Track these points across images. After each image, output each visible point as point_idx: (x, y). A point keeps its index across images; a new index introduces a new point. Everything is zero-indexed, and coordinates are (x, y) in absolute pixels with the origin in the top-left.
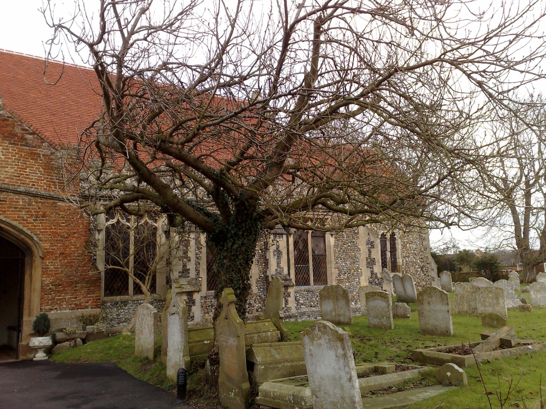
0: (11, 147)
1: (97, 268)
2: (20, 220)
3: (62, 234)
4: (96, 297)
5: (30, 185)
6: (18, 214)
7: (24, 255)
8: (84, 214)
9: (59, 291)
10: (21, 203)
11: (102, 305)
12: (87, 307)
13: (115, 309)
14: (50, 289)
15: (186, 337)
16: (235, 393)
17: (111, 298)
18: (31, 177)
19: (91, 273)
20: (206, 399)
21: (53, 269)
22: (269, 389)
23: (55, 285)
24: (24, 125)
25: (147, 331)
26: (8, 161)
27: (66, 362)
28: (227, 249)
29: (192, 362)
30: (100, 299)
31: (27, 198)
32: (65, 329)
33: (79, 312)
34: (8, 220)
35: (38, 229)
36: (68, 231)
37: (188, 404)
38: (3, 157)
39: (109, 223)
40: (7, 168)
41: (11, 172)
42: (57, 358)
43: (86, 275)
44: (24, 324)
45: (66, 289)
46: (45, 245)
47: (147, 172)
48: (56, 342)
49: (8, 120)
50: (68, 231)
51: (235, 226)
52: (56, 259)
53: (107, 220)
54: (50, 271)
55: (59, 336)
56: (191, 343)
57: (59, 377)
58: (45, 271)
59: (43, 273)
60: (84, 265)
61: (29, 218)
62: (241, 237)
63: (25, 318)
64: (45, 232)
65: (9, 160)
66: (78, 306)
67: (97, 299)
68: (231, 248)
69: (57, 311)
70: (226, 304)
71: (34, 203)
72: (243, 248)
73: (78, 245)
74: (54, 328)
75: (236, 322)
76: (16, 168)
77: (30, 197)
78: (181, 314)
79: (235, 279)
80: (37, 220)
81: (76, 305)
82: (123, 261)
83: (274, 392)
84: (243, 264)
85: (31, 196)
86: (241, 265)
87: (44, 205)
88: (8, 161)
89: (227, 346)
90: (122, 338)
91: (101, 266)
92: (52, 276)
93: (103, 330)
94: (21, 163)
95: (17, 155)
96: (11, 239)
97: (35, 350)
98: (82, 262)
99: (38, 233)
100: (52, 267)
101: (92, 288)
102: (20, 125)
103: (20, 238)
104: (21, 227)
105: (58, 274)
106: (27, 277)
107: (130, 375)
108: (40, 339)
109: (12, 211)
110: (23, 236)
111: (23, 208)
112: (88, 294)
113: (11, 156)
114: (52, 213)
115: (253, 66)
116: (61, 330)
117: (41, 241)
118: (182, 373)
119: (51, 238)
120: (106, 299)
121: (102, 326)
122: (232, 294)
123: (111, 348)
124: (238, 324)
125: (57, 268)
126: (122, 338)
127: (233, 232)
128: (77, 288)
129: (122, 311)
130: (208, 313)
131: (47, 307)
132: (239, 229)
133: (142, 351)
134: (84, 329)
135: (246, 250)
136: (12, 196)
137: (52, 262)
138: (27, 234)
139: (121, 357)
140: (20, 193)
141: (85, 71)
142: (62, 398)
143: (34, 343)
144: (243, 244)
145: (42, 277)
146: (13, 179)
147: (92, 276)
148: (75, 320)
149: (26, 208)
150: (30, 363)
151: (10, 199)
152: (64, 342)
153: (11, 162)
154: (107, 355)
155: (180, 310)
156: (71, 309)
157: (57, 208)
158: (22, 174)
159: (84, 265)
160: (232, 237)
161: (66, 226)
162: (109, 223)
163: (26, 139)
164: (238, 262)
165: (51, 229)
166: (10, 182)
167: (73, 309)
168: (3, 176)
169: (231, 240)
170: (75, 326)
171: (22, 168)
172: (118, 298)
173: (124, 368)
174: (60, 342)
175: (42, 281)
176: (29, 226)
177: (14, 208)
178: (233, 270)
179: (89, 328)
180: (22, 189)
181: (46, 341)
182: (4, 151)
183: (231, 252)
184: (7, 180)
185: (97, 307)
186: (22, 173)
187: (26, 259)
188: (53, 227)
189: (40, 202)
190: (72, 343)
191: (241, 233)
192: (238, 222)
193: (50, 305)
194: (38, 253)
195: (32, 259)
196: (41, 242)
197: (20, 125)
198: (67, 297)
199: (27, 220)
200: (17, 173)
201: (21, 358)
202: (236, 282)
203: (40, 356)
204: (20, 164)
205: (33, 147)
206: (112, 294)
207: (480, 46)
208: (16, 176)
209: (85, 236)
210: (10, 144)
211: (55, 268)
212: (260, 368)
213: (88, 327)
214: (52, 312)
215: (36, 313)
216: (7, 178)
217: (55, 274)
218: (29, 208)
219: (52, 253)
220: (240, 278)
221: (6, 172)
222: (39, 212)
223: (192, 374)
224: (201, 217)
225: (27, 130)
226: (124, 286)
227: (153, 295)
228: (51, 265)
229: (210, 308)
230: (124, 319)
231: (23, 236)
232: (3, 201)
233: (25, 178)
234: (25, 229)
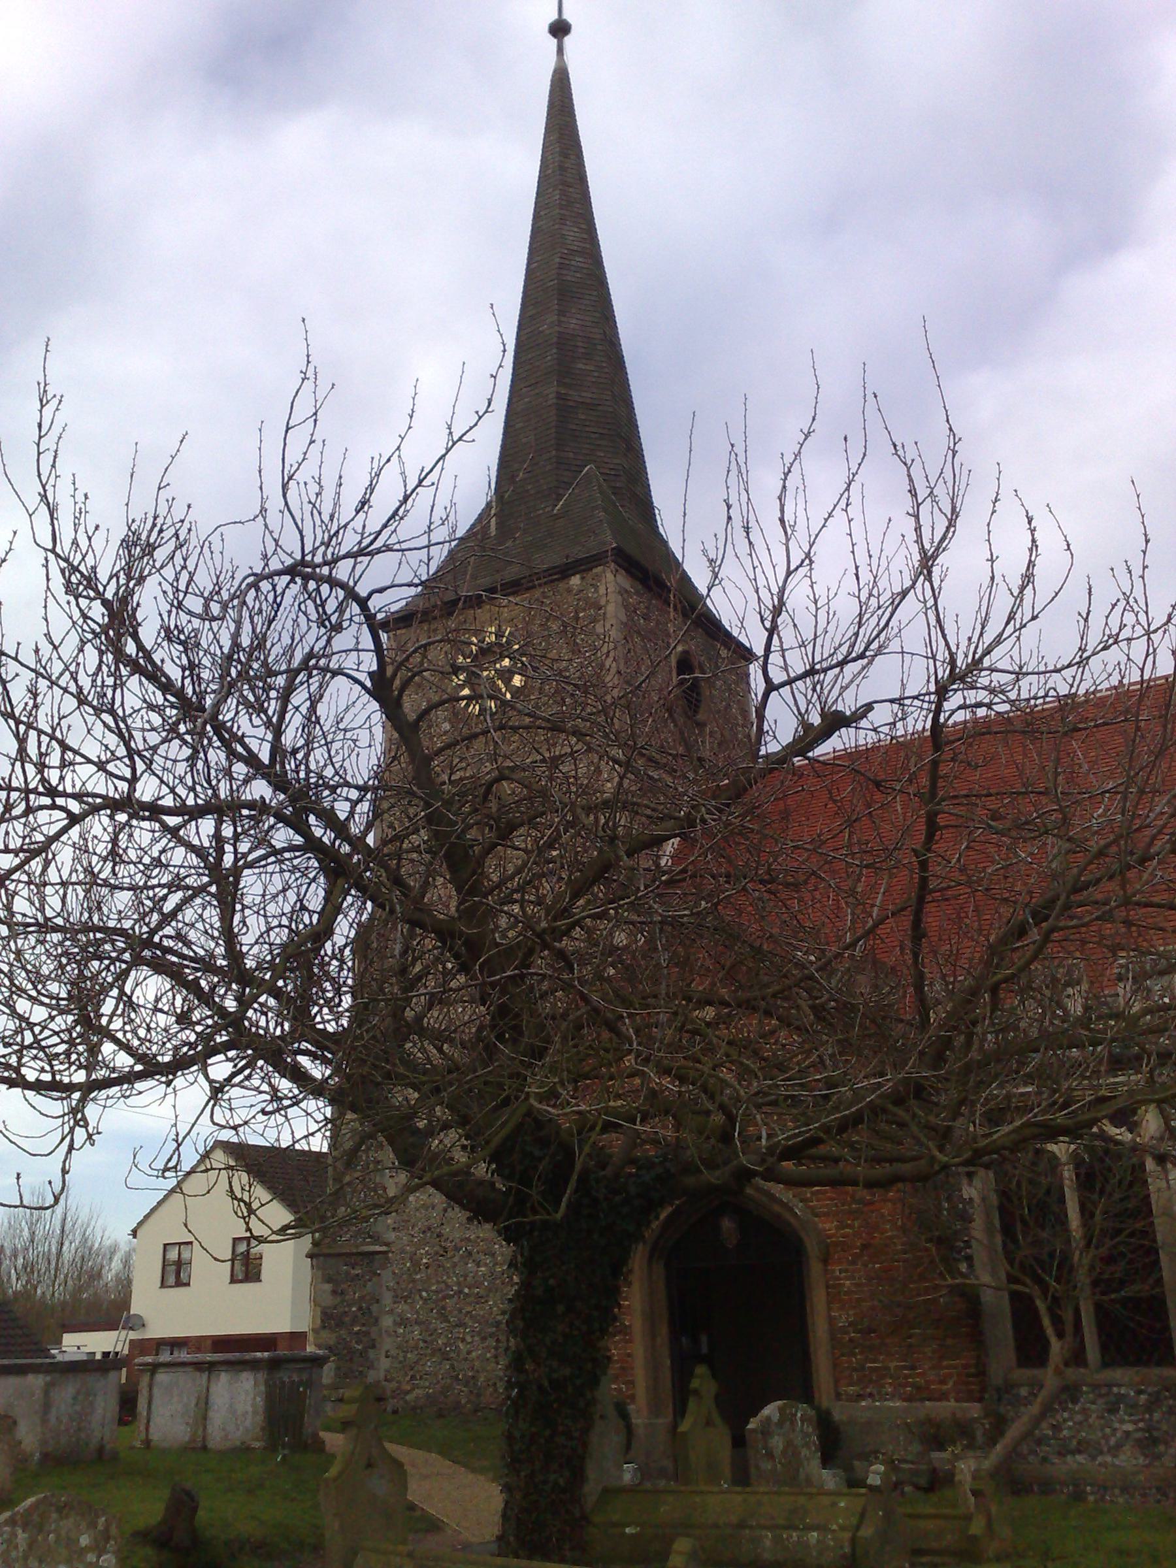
12: (943, 1397)
46: (827, 1226)
52: (853, 1263)
54: (846, 1293)
66: (922, 1393)
81: (918, 1388)
101: (949, 1342)
117: (816, 1215)
119: (836, 1205)
129: (1066, 1415)
194: (812, 1248)
198: (892, 1365)
207: (165, 779)
211: (857, 1285)
214: (863, 1404)
224: (1036, 1130)
228: (846, 1278)
230: (1074, 1442)
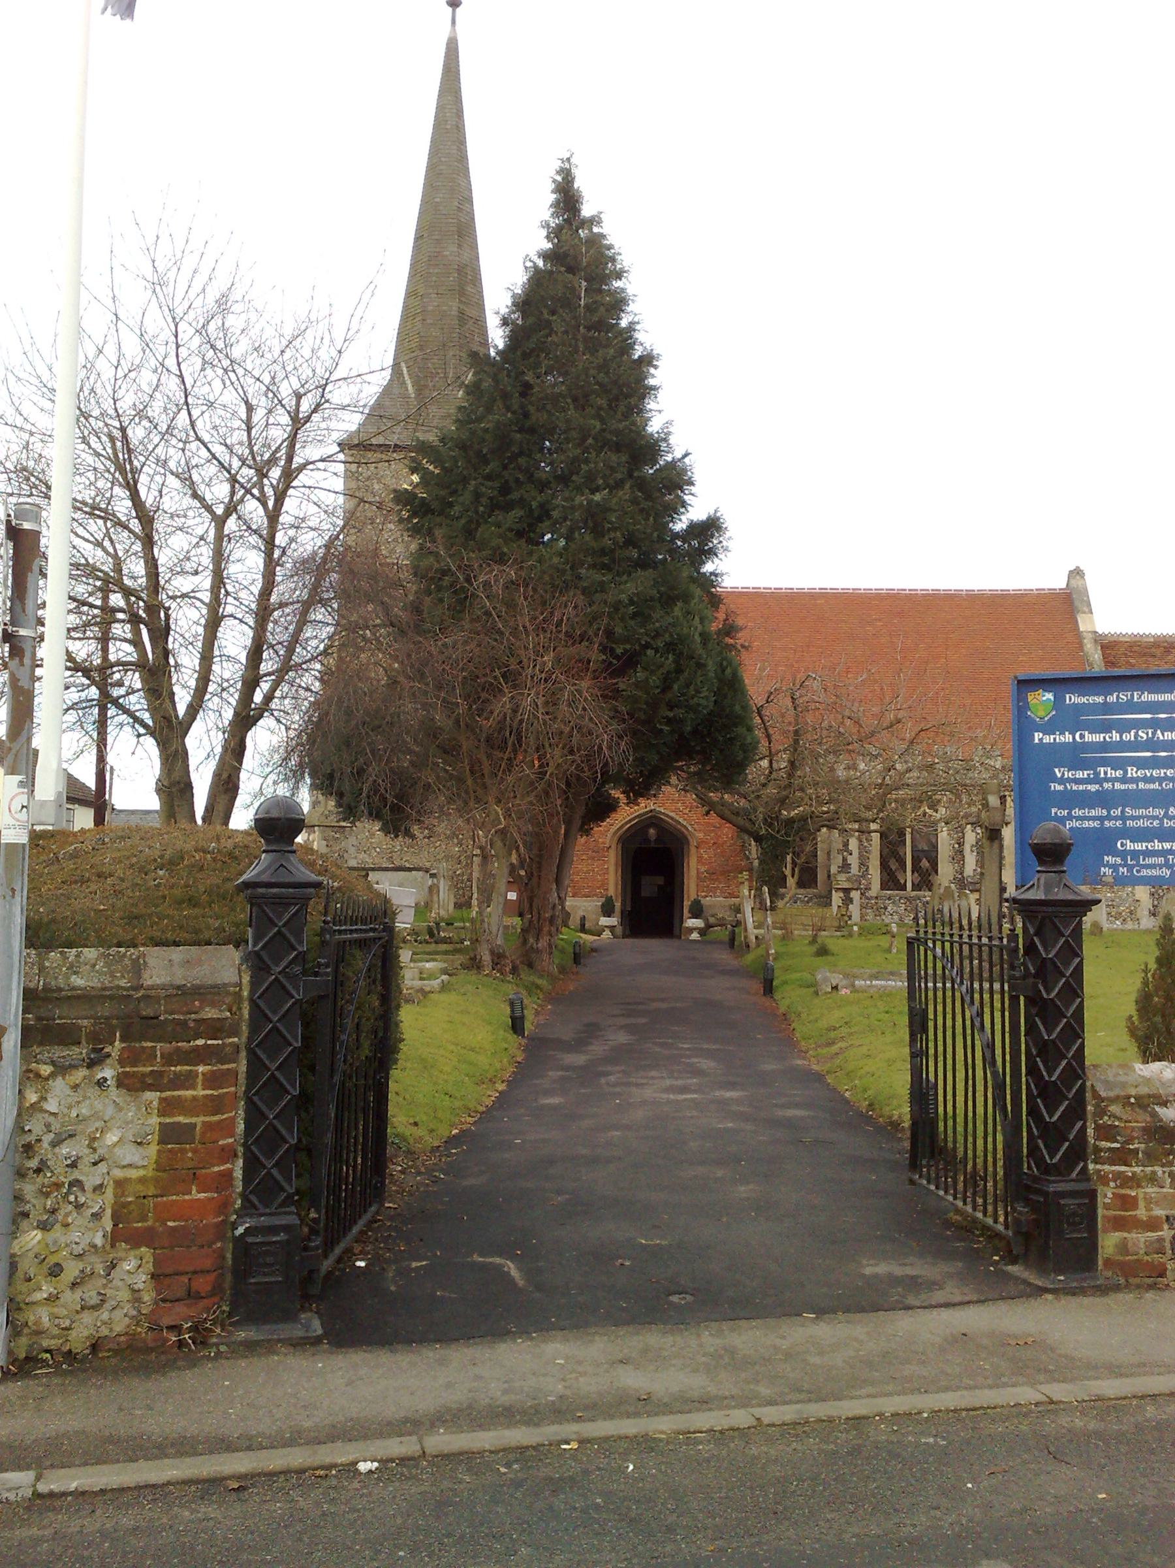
34: (667, 812)
48: (709, 926)
55: (712, 920)
58: (700, 860)
74: (707, 912)
97: (691, 930)
104: (677, 818)
116: (713, 916)
131: (703, 894)
170: (728, 913)
194: (693, 843)
203: (695, 936)
215: (693, 896)
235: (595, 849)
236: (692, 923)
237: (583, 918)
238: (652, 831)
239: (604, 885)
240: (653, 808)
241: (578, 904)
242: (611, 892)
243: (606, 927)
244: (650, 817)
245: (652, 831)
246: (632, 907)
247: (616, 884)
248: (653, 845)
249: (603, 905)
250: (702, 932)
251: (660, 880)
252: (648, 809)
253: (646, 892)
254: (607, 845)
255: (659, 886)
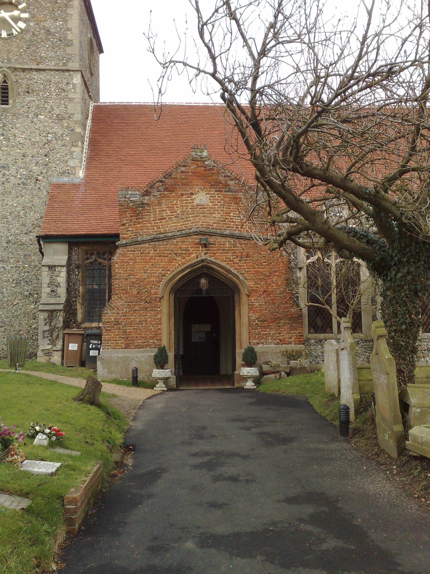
0: (217, 194)
1: (298, 305)
2: (227, 261)
3: (264, 273)
4: (299, 333)
5: (235, 229)
6: (226, 256)
7: (233, 293)
8: (284, 253)
9: (264, 327)
10: (227, 245)
11: (307, 341)
12: (290, 343)
13: (320, 346)
14: (256, 324)
15: (355, 374)
16: (389, 436)
17: (316, 335)
18: (234, 220)
19: (293, 310)
20: (367, 439)
21: (258, 306)
22: (418, 434)
23: (260, 321)
24: (227, 172)
25: (332, 367)
26: (215, 208)
27: (268, 392)
28: (391, 279)
29: (361, 401)
30: (302, 336)
31: (232, 240)
32: (270, 362)
33: (284, 347)
34: (218, 262)
35: (243, 269)
36: (269, 270)
37: (349, 442)
38: (211, 204)
39: (309, 261)
40: (215, 213)
41: (218, 218)
42: (262, 388)
43: (288, 311)
44: (237, 355)
45: (271, 324)
46: (250, 283)
47: (294, 200)
48: (263, 373)
49: (213, 169)
50: (269, 270)
51: (399, 252)
53: (308, 258)
54: (255, 308)
55: (266, 368)
56: (362, 380)
57: (251, 404)
58: (251, 308)
59: (250, 309)
60: (286, 303)
61: (235, 258)
62: (406, 264)
63: (238, 350)
64: (249, 271)
65: (216, 207)
66: (282, 342)
67: (300, 336)
68: (395, 278)
69: (264, 345)
70: (376, 338)
71: (238, 245)
72: (409, 278)
73: (279, 283)
74: (260, 360)
75: (385, 357)
76: (222, 214)
77: (235, 240)
78: (348, 349)
79: (399, 312)
80: (242, 260)
81: (281, 340)
82: (323, 298)
83: (422, 437)
84: (409, 296)
85: (236, 238)
86: (407, 297)
87: (247, 246)
88: (215, 208)
89: (379, 384)
90: (320, 375)
91: (303, 303)
92: (257, 312)
93: (306, 366)
94: (226, 208)
95: (222, 201)
96: (220, 277)
97: (245, 379)
98: (284, 299)
99: (244, 272)
100: (257, 304)
101: (294, 325)
102: (223, 173)
103: (229, 278)
104: (228, 267)
105: (263, 310)
106: (237, 313)
107: (314, 409)
108: (248, 369)
109: (221, 253)
110: (230, 276)
111: (230, 250)
112: (291, 330)
113: (218, 202)
114: (254, 253)
115: (397, 57)
116: (267, 363)
117: (246, 279)
118: (343, 409)
119: (255, 276)
120: (310, 336)
121: (304, 362)
122: (381, 327)
123: (308, 383)
124: (388, 359)
125: (261, 305)
126: (320, 375)
127: (396, 259)
128: (280, 324)
130: (424, 358)
131: (255, 341)
132: (404, 255)
133: (330, 388)
134: (289, 363)
135: (413, 279)
136: (220, 239)
137: (257, 300)
138: (234, 273)
139: (315, 392)
140: (226, 236)
141: (221, 108)
142: (242, 420)
143: (243, 373)
144: (408, 273)
145: (249, 313)
146: (220, 224)
147: (294, 313)
148: (280, 354)
149: (232, 250)
150: (242, 390)
151: (218, 242)
152: (271, 374)
153: (218, 208)
154: (303, 390)
155: (348, 345)
156: (275, 344)
157: (259, 248)
158: (227, 219)
159: (286, 303)
160: (395, 265)
161: (268, 265)
162: (309, 261)
163: (229, 185)
164: (403, 294)
165: (255, 268)
166: (218, 226)
167: (278, 344)
168: (211, 222)
169: (395, 268)
170: (280, 360)
171: (227, 213)
172: (322, 336)
173: (311, 403)
174: (267, 374)
175: (249, 317)
176: (235, 266)
177: (223, 250)
178: (397, 303)
179: (293, 363)
180: (227, 232)
181: (252, 371)
182: (211, 198)
183: (395, 282)
184: (215, 225)
185: (300, 343)
186: (227, 217)
187: (236, 296)
188: (256, 267)
189: (243, 243)
190: (278, 375)
191: (405, 260)
192: (401, 246)
193: (257, 339)
194: (244, 291)
195: (240, 297)
196: (246, 281)
197: (223, 173)
198: (272, 333)
199: (233, 261)
200: (223, 218)
201: (236, 385)
202: (400, 316)
203: (250, 385)
204: (225, 209)
205: (236, 192)
206: (316, 332)
208: (222, 221)
209: (285, 274)
210: (216, 191)
211: (260, 305)
212: (414, 411)
213: (291, 362)
214: (260, 346)
215: (245, 345)
216: (215, 223)
217: (260, 310)
218: (235, 250)
219: (256, 291)
220: (406, 312)
221: (213, 217)
222: (243, 252)
223: (361, 412)
225: (229, 176)
226: (328, 324)
227: (356, 335)
228: (256, 302)
229: (426, 352)
231: (230, 276)
232: (213, 244)
233: (230, 222)
234: (232, 269)
235: (148, 300)
236: (246, 371)
237: (135, 371)
238: (203, 281)
239: (157, 335)
240: (204, 257)
241: (131, 355)
242: (165, 342)
243: (159, 379)
244: (203, 267)
245: (203, 281)
246: (245, 389)
247: (170, 334)
248: (204, 295)
249: (156, 357)
250: (257, 381)
251: (207, 328)
252: (199, 259)
253: (195, 338)
254: (160, 296)
255: (207, 333)
